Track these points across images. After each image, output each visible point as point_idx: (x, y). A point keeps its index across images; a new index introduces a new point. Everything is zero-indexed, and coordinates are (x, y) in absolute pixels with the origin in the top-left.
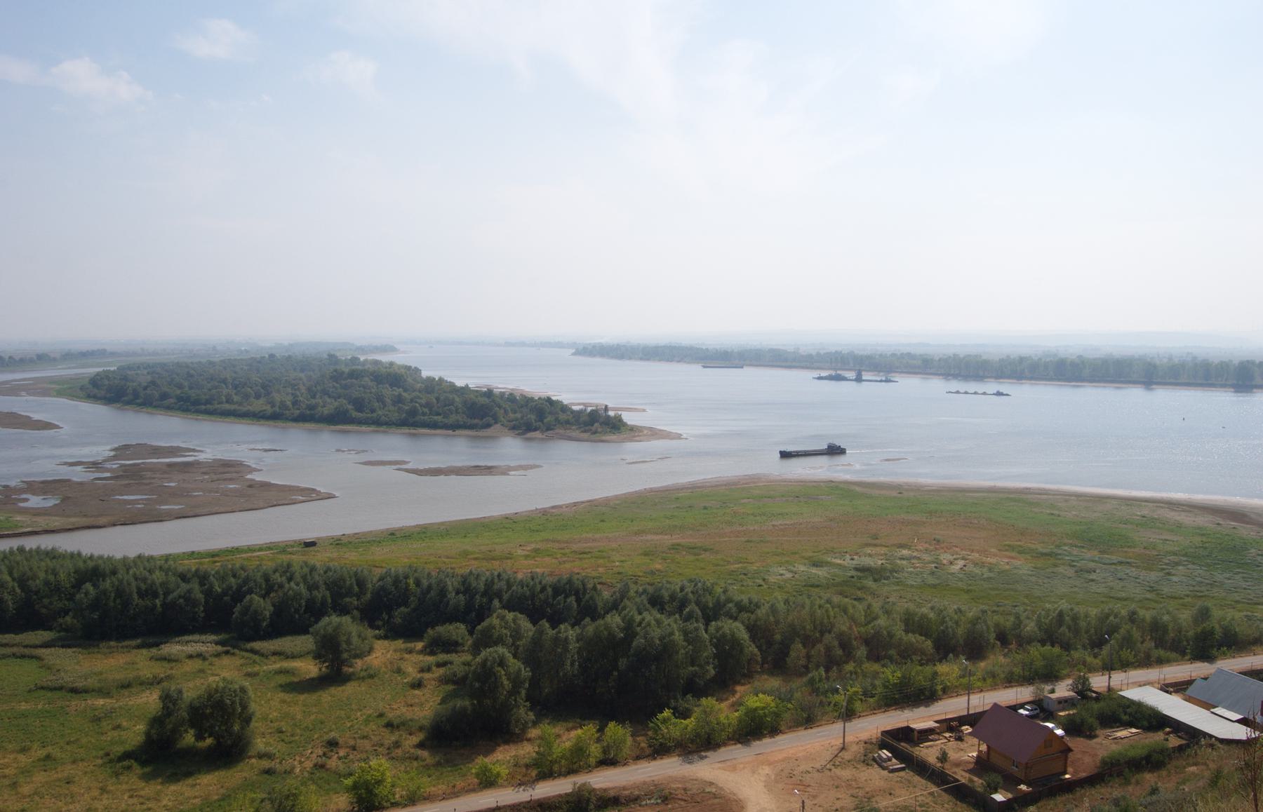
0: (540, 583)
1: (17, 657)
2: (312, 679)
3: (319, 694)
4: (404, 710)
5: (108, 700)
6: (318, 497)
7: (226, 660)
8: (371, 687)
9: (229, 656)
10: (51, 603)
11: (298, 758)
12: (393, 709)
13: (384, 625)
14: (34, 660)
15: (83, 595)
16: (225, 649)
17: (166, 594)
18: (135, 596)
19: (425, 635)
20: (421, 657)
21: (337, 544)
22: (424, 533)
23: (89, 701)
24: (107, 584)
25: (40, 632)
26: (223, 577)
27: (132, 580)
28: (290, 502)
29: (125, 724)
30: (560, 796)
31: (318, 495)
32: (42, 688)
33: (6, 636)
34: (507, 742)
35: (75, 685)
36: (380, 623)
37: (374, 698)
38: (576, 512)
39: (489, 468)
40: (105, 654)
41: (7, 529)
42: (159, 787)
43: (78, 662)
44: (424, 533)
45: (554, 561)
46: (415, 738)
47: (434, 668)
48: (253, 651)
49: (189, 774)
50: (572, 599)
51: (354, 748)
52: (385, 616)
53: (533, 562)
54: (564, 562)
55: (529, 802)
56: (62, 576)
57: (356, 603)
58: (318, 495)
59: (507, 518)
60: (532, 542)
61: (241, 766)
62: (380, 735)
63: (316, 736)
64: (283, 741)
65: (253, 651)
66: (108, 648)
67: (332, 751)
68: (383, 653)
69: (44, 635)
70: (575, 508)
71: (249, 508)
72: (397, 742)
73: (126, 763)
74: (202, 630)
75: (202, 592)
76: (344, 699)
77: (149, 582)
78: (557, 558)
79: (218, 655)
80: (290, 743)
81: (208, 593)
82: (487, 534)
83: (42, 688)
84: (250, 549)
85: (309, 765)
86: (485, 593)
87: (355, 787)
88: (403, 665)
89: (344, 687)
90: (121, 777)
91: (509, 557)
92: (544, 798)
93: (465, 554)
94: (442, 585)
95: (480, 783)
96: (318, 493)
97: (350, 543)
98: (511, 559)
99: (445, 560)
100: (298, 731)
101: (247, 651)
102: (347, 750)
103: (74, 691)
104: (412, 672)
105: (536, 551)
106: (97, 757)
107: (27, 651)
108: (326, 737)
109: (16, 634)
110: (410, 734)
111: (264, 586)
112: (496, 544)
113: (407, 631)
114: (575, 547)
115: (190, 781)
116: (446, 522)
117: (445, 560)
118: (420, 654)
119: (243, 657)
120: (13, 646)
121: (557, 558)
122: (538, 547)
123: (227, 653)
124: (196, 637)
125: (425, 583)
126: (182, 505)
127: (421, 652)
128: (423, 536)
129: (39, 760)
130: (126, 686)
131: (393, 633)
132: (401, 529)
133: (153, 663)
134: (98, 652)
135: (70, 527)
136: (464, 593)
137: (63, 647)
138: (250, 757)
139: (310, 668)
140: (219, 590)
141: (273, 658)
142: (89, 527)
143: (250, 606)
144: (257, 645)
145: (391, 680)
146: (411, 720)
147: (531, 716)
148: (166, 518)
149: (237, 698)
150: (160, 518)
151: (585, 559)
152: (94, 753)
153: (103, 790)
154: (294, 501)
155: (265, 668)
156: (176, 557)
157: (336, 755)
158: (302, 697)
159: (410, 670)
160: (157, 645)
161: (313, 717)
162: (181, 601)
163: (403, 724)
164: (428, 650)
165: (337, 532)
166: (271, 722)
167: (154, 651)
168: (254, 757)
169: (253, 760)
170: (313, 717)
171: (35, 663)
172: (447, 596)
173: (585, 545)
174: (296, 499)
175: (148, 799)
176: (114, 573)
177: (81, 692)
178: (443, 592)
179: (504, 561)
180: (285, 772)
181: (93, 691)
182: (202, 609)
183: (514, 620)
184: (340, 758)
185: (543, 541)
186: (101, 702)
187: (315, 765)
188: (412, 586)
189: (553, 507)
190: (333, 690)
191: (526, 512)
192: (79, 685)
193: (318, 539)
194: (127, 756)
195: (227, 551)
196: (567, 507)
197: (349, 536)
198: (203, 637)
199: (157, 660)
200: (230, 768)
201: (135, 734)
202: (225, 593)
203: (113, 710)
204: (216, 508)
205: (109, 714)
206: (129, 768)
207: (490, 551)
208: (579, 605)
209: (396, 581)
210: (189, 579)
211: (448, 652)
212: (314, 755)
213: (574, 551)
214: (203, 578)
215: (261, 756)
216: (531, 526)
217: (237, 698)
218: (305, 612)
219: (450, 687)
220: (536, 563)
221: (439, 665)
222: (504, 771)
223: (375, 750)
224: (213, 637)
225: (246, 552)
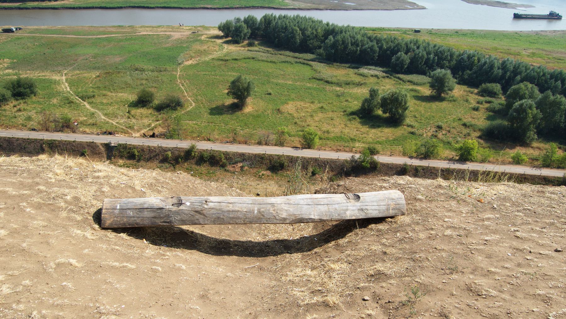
0: (543, 71)
1: (301, 64)
2: (427, 96)
3: (431, 103)
4: (470, 119)
5: (341, 89)
6: (418, 8)
7: (387, 80)
8: (454, 106)
9: (388, 78)
10: (313, 43)
11: (424, 130)
12: (465, 118)
13: (459, 78)
14: (308, 66)
15: (329, 41)
16: (387, 75)
17: (362, 46)
18: (350, 45)
19: (480, 86)
20: (477, 97)
21: (430, 33)
22: (473, 34)
23: (333, 88)
24: (339, 37)
25: (309, 54)
26: (387, 42)
27: (349, 37)
28: (404, 8)
29: (349, 100)
30: (554, 177)
31: (417, 7)
32: (315, 78)
33: (296, 54)
34: (521, 146)
35: (327, 80)
36: (458, 76)
37: (456, 111)
38: (555, 36)
39: (506, 4)
40: (336, 68)
41: (284, 6)
42: (368, 129)
43: (326, 70)
44: (473, 34)
45: (543, 61)
46: (476, 134)
47: (484, 103)
48: (399, 78)
49: (379, 127)
50: (559, 83)
51: (449, 132)
52: (460, 73)
53: (532, 59)
54: (549, 62)
55: (539, 176)
56: (319, 30)
57: (447, 64)
58: (417, 7)
59: (516, 33)
60: (530, 49)
61: (400, 128)
62: (460, 128)
63: (431, 122)
64: (417, 121)
65: (399, 78)
66: (337, 66)
67: (439, 130)
68: (458, 91)
69: (310, 56)
70: (554, 33)
71: (385, 9)
72: (469, 133)
73: (354, 116)
74: (376, 65)
75: (378, 47)
76: (442, 108)
77: (356, 39)
78: (545, 60)
79: (384, 77)
80: (420, 123)
81: (381, 48)
82: (506, 40)
83: (315, 78)
84: (389, 30)
85: (430, 134)
86: (513, 72)
87: (461, 149)
88: (469, 98)
89: (441, 103)
90: (352, 122)
91: (519, 54)
92: (547, 176)
93: (496, 49)
94: (492, 63)
95: (513, 162)
96: (418, 6)
97: (436, 34)
98: (520, 55)
99: (485, 50)
100: (423, 118)
101: (396, 78)
102: (446, 132)
103: (327, 82)
104: (474, 104)
105: (533, 54)
106: (341, 111)
107: (306, 62)
108: (436, 124)
109: (300, 53)
110: (475, 131)
111: (405, 49)
112: (511, 46)
113: (470, 83)
114: (555, 55)
115: (380, 129)
116: (483, 30)
117: (485, 50)
118: (476, 95)
119: (395, 80)
120: (299, 58)
121: (545, 60)
122: (534, 51)
123: (388, 77)
124: (373, 67)
125: (483, 61)
126: (354, 3)
127: (476, 94)
128: (472, 35)
129: (319, 108)
130: (348, 84)
131: (462, 82)
132: (461, 30)
133: (356, 76)
134: (333, 67)
135: (309, 8)
136: (502, 69)
137: (319, 62)
138: (404, 125)
139: (426, 91)
140: (385, 48)
141: (408, 83)
142: (316, 9)
143: (400, 57)
144: (401, 76)
145: (464, 105)
146: (474, 125)
147: (536, 137)
148: (349, 9)
149: (404, 98)
150: (346, 9)
151: (561, 63)
152: (340, 110)
153: (346, 125)
154: (406, 8)
155: (405, 87)
156: (367, 29)
157: (441, 133)
158: (424, 104)
159: (472, 101)
160: (357, 68)
161: (429, 114)
162: (369, 49)
163: (471, 126)
164: (480, 94)
165: (430, 27)
166: (411, 112)
167: (356, 70)
168: (405, 125)
169: (405, 127)
170: (429, 114)
171: (309, 68)
172: (493, 70)
173: (560, 55)
174: (407, 7)
175: (364, 133)
176: (341, 32)
177: (329, 83)
178: (492, 66)
179: (516, 56)
180: (420, 135)
181: (335, 83)
182: (377, 54)
183: (531, 88)
184: (443, 135)
185: (536, 49)
186: (338, 89)
187: (432, 135)
188: (476, 61)
189: (542, 31)
190: (437, 103)
191: (527, 31)
192: (330, 79)
193: (421, 29)
194: (353, 113)
195: (379, 29)
196: (550, 32)
197: (435, 30)
198: (377, 68)
199: (358, 75)
200: (396, 128)
201: (356, 105)
202: (388, 49)
203: (344, 93)
204: (370, 7)
205: (343, 94)
206: (355, 119)
207: (508, 50)
208: (562, 87)
209: (469, 57)
210: (372, 40)
211: (491, 97)
212: (431, 131)
213: (554, 58)
214: (378, 41)
215: (408, 126)
216: (530, 39)
217: (404, 98)
218: (424, 64)
219: (491, 114)
220: (534, 60)
221: (487, 102)
222: (525, 158)
223: (459, 135)
224: (380, 69)
225: (388, 31)
